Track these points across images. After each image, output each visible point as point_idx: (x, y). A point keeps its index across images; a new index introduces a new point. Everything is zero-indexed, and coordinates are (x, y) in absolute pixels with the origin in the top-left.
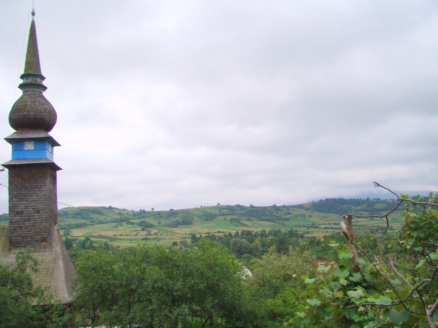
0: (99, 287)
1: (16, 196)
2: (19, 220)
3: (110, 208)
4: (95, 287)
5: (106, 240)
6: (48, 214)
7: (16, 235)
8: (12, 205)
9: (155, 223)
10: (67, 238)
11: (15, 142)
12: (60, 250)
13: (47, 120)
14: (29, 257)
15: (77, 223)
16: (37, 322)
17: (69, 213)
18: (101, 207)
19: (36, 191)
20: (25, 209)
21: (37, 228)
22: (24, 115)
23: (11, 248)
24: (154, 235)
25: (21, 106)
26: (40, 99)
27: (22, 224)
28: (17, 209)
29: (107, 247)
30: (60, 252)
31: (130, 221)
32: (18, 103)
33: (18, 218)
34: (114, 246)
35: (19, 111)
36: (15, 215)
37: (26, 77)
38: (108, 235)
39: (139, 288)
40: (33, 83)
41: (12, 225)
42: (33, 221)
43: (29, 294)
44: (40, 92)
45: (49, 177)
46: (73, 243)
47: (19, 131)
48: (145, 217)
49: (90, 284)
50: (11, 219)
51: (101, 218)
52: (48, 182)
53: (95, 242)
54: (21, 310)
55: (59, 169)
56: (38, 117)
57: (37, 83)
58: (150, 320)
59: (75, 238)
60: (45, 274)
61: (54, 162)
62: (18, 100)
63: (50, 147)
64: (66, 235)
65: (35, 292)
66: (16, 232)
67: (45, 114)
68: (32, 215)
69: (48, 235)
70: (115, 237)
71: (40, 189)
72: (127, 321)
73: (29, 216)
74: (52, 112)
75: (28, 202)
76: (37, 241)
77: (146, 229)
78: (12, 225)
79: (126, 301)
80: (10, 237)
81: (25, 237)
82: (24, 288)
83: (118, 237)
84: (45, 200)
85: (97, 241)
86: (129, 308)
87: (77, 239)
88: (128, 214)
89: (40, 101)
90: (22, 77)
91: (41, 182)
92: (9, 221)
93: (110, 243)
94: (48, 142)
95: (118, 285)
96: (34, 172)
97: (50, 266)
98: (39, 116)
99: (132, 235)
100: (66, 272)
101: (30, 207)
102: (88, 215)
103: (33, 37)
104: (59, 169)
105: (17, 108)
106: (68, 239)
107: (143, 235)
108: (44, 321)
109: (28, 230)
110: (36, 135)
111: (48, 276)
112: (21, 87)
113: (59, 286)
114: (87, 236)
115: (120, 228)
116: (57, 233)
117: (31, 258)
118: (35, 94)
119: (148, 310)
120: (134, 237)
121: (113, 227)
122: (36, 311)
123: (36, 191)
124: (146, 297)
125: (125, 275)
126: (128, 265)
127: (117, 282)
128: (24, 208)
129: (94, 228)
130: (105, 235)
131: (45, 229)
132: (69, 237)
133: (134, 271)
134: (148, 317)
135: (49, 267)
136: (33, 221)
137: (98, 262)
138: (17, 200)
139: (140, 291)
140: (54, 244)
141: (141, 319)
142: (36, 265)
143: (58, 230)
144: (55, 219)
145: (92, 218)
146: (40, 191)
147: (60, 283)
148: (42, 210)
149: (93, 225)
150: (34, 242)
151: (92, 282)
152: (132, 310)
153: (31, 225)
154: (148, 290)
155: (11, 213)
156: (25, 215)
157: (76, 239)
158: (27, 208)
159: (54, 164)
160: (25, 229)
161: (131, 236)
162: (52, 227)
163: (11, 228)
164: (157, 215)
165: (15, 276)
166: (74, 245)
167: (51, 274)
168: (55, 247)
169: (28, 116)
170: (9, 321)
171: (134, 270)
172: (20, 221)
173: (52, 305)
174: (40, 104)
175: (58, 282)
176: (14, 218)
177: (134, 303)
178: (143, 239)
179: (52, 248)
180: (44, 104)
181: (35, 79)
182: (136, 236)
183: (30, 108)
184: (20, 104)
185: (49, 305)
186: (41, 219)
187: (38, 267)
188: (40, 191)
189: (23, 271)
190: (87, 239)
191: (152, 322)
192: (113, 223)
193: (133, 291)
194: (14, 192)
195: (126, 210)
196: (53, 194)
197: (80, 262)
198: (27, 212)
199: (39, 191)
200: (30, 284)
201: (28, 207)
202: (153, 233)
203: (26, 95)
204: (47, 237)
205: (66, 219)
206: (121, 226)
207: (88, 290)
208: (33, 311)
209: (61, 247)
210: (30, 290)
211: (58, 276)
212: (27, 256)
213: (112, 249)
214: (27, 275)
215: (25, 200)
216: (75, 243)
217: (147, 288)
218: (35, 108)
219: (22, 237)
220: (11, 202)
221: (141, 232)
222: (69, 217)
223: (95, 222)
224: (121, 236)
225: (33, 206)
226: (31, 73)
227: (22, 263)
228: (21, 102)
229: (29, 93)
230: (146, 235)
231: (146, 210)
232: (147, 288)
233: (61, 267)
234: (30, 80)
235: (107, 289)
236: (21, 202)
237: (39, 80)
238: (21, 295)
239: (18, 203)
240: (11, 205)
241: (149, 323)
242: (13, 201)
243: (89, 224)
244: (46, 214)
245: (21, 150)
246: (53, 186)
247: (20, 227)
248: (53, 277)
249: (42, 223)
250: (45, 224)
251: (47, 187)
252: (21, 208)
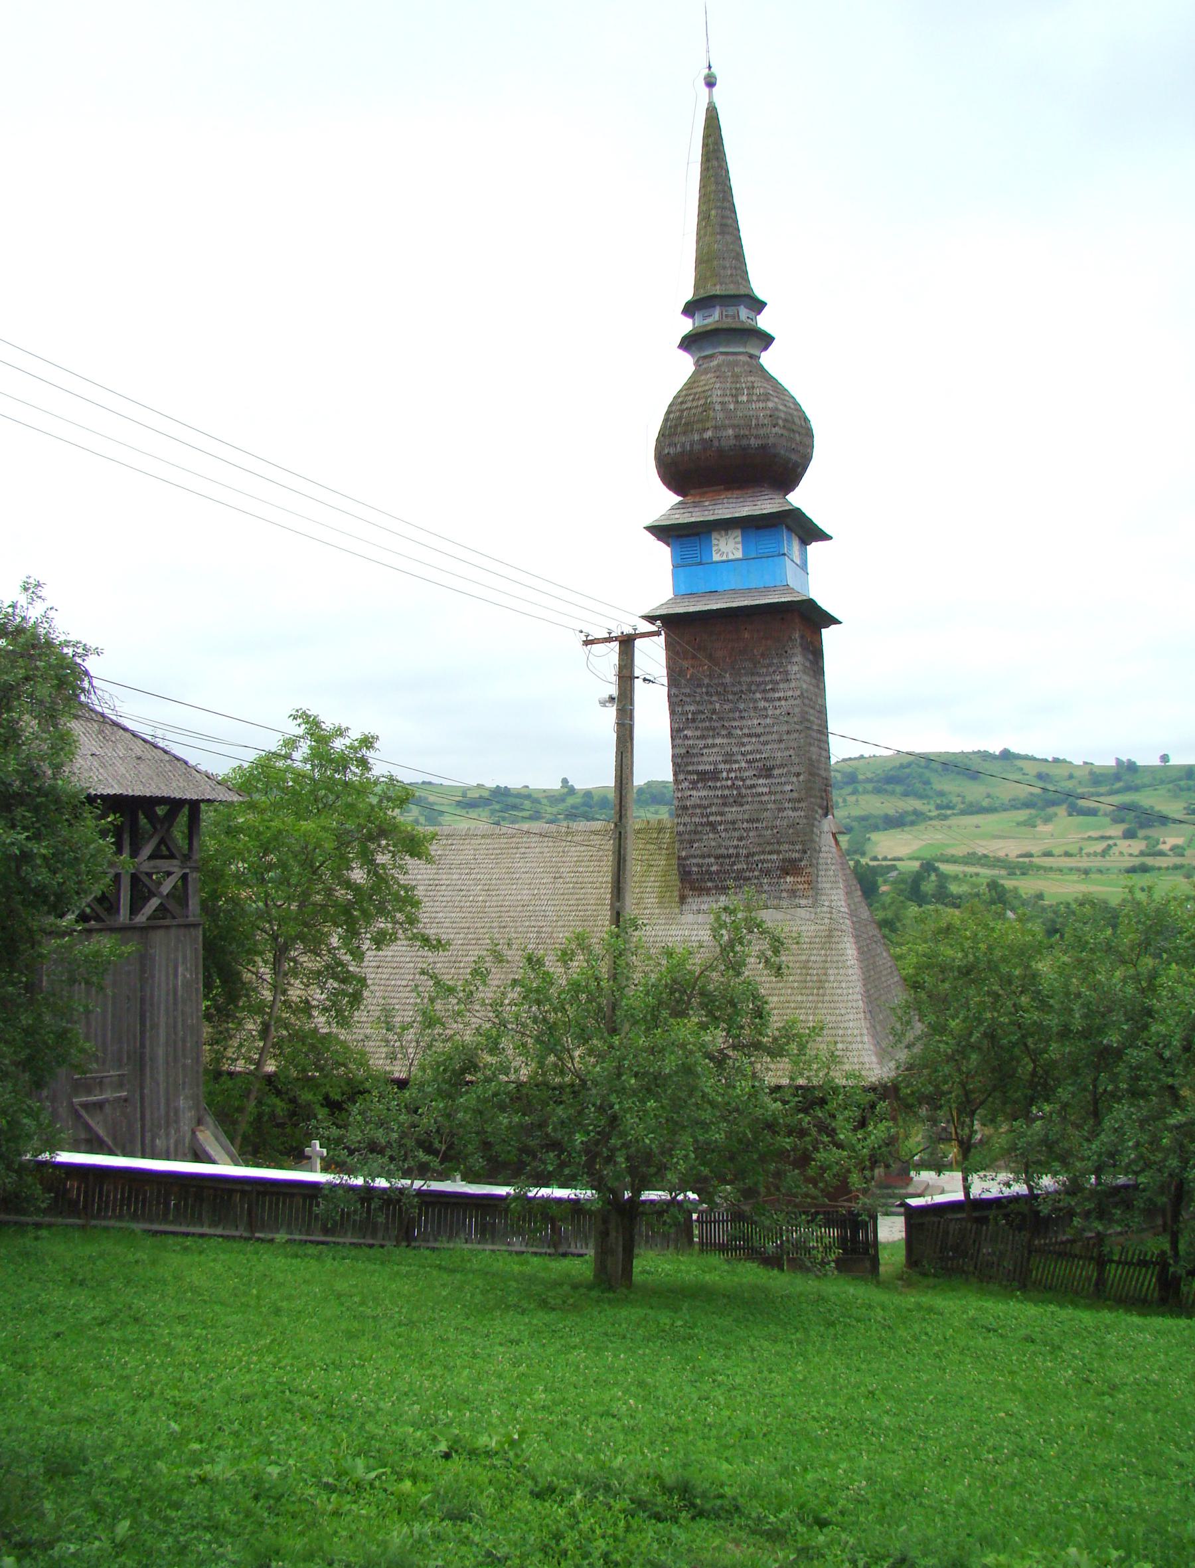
0: (985, 1035)
1: (694, 720)
2: (705, 802)
3: (1006, 755)
4: (971, 1034)
5: (996, 872)
6: (801, 778)
7: (698, 852)
8: (683, 751)
9: (1174, 808)
10: (857, 862)
11: (679, 536)
12: (843, 903)
13: (782, 452)
14: (753, 925)
15: (891, 812)
16: (787, 1140)
17: (861, 777)
18: (974, 753)
19: (756, 701)
20: (725, 762)
21: (767, 828)
22: (703, 440)
23: (686, 892)
24: (1170, 853)
25: (693, 411)
26: (752, 379)
27: (716, 814)
28: (699, 763)
29: (999, 897)
30: (846, 910)
31: (1082, 803)
32: (682, 403)
33: (703, 793)
34: (1022, 892)
35: (688, 427)
36: (694, 783)
37: (699, 309)
38: (1001, 854)
39: (1131, 1046)
40: (725, 326)
41: (687, 819)
42: (752, 802)
43: (757, 1046)
44: (751, 356)
45: (798, 650)
46: (880, 880)
47: (689, 499)
48: (1136, 789)
49: (953, 1024)
50: (680, 799)
51: (975, 792)
52: (795, 668)
53: (956, 878)
54: (738, 1096)
55: (831, 620)
56: (749, 445)
57: (738, 326)
58: (1173, 1162)
59: (884, 863)
60: (796, 985)
61: (813, 595)
62: (681, 391)
63: (796, 545)
64: (855, 852)
65: (775, 1039)
66: (698, 841)
67: (774, 430)
68: (748, 782)
69: (805, 852)
70: (1027, 860)
71: (770, 695)
72: (1089, 1158)
73: (738, 788)
74: (796, 420)
75: (733, 741)
76: (767, 873)
77: (1141, 833)
78: (687, 819)
79: (1085, 1089)
80: (679, 858)
81: (730, 856)
82: (742, 1027)
83: (1036, 860)
84: (788, 732)
85: (961, 876)
86: (1097, 1115)
87: (894, 868)
88: (1071, 777)
89: (753, 387)
90: (690, 309)
91: (771, 670)
92: (676, 802)
93: (1009, 884)
94: (789, 529)
95: (1055, 1030)
96: (747, 635)
97: (813, 958)
98: (753, 441)
99: (1088, 855)
100: (867, 980)
101: (739, 757)
102: (927, 783)
103: (715, 163)
104: (831, 620)
105: (681, 418)
106: (862, 866)
107: (1131, 855)
108: (808, 1139)
109: (736, 834)
110: (746, 509)
111: (808, 991)
112: (689, 343)
113: (846, 1025)
114: (927, 855)
115: (1042, 828)
116: (833, 841)
117: (758, 926)
118: (736, 363)
119: (1165, 1124)
120: (1098, 862)
121: (1018, 824)
122: (785, 1102)
123: (756, 701)
124: (1159, 1080)
125: (1079, 995)
126: (1091, 961)
127: (1052, 1021)
128: (720, 758)
129: (950, 827)
130: (991, 855)
131: (791, 831)
132: (863, 861)
133: (1114, 981)
134: (1168, 1151)
135: (808, 961)
136: (752, 802)
137: (983, 946)
138: (698, 733)
139: (1135, 1055)
140: (825, 884)
141: (1141, 1157)
142: (776, 952)
143: (834, 835)
144: (822, 798)
145: (941, 794)
146: (773, 700)
147: (847, 1017)
148: (781, 766)
149: (946, 817)
150: (756, 873)
151: (961, 1016)
152: (1107, 1124)
153: (746, 817)
154: (1167, 1054)
155: (681, 777)
156: (724, 783)
157: (888, 866)
158: (729, 758)
159: (811, 603)
160: (725, 830)
161: (1085, 859)
162: (816, 823)
163: (681, 828)
164: (1180, 779)
165: (711, 987)
166: (884, 888)
167: (818, 984)
168: (828, 892)
169: (716, 443)
170: (705, 1126)
171: (1114, 978)
172: (710, 805)
173: (835, 1090)
174: (755, 398)
175: (843, 1011)
176: (692, 793)
177: (1115, 1097)
178: (1132, 870)
179: (817, 894)
180: (766, 397)
181: (731, 311)
182: (1103, 856)
183: (720, 415)
184: (689, 405)
185: (917, 1062)
186: (778, 797)
187: (784, 958)
188: (773, 700)
189: (736, 967)
190: (928, 867)
191: (1184, 1169)
192: (1018, 809)
193: (1107, 1057)
194: (687, 708)
195: (1064, 761)
196: (811, 711)
197: (913, 950)
198: (733, 775)
199: (766, 700)
200: (759, 1013)
201: (734, 758)
202: (1165, 848)
203: (706, 372)
204: (801, 860)
205: (853, 798)
206: (1047, 820)
207: (947, 1043)
208: (775, 1102)
209: (848, 894)
210: (761, 1034)
211: (839, 991)
212: (746, 919)
213: (1016, 903)
214: (749, 984)
215: (724, 732)
216: (885, 881)
217: (1165, 1046)
218: (739, 414)
219: (717, 857)
220: (678, 741)
221: (1123, 845)
222: (860, 790)
223: (952, 808)
224: (1050, 859)
225: (751, 753)
226: (718, 293)
227: (731, 943)
228: (691, 398)
229: (715, 363)
230: (1142, 854)
231: (1140, 762)
232: (1165, 1046)
233: (849, 963)
234: (714, 318)
235: (1014, 1045)
236: (710, 741)
237: (744, 313)
238: (734, 1047)
239: (701, 743)
240: (678, 751)
241: (1170, 1175)
242: (686, 737)
243: (933, 814)
244: (794, 779)
245: (701, 564)
246: (814, 681)
247: (710, 824)
248: (823, 995)
249: (780, 810)
250: (790, 813)
251: (793, 685)
252: (711, 759)
